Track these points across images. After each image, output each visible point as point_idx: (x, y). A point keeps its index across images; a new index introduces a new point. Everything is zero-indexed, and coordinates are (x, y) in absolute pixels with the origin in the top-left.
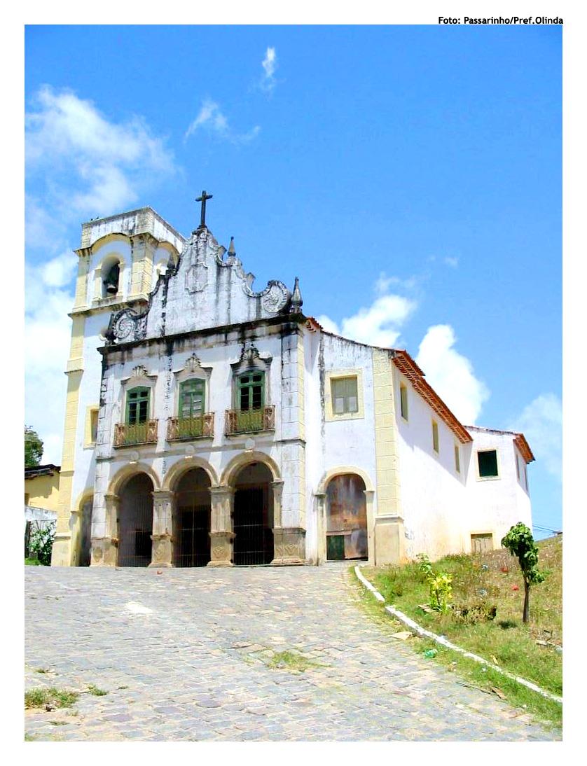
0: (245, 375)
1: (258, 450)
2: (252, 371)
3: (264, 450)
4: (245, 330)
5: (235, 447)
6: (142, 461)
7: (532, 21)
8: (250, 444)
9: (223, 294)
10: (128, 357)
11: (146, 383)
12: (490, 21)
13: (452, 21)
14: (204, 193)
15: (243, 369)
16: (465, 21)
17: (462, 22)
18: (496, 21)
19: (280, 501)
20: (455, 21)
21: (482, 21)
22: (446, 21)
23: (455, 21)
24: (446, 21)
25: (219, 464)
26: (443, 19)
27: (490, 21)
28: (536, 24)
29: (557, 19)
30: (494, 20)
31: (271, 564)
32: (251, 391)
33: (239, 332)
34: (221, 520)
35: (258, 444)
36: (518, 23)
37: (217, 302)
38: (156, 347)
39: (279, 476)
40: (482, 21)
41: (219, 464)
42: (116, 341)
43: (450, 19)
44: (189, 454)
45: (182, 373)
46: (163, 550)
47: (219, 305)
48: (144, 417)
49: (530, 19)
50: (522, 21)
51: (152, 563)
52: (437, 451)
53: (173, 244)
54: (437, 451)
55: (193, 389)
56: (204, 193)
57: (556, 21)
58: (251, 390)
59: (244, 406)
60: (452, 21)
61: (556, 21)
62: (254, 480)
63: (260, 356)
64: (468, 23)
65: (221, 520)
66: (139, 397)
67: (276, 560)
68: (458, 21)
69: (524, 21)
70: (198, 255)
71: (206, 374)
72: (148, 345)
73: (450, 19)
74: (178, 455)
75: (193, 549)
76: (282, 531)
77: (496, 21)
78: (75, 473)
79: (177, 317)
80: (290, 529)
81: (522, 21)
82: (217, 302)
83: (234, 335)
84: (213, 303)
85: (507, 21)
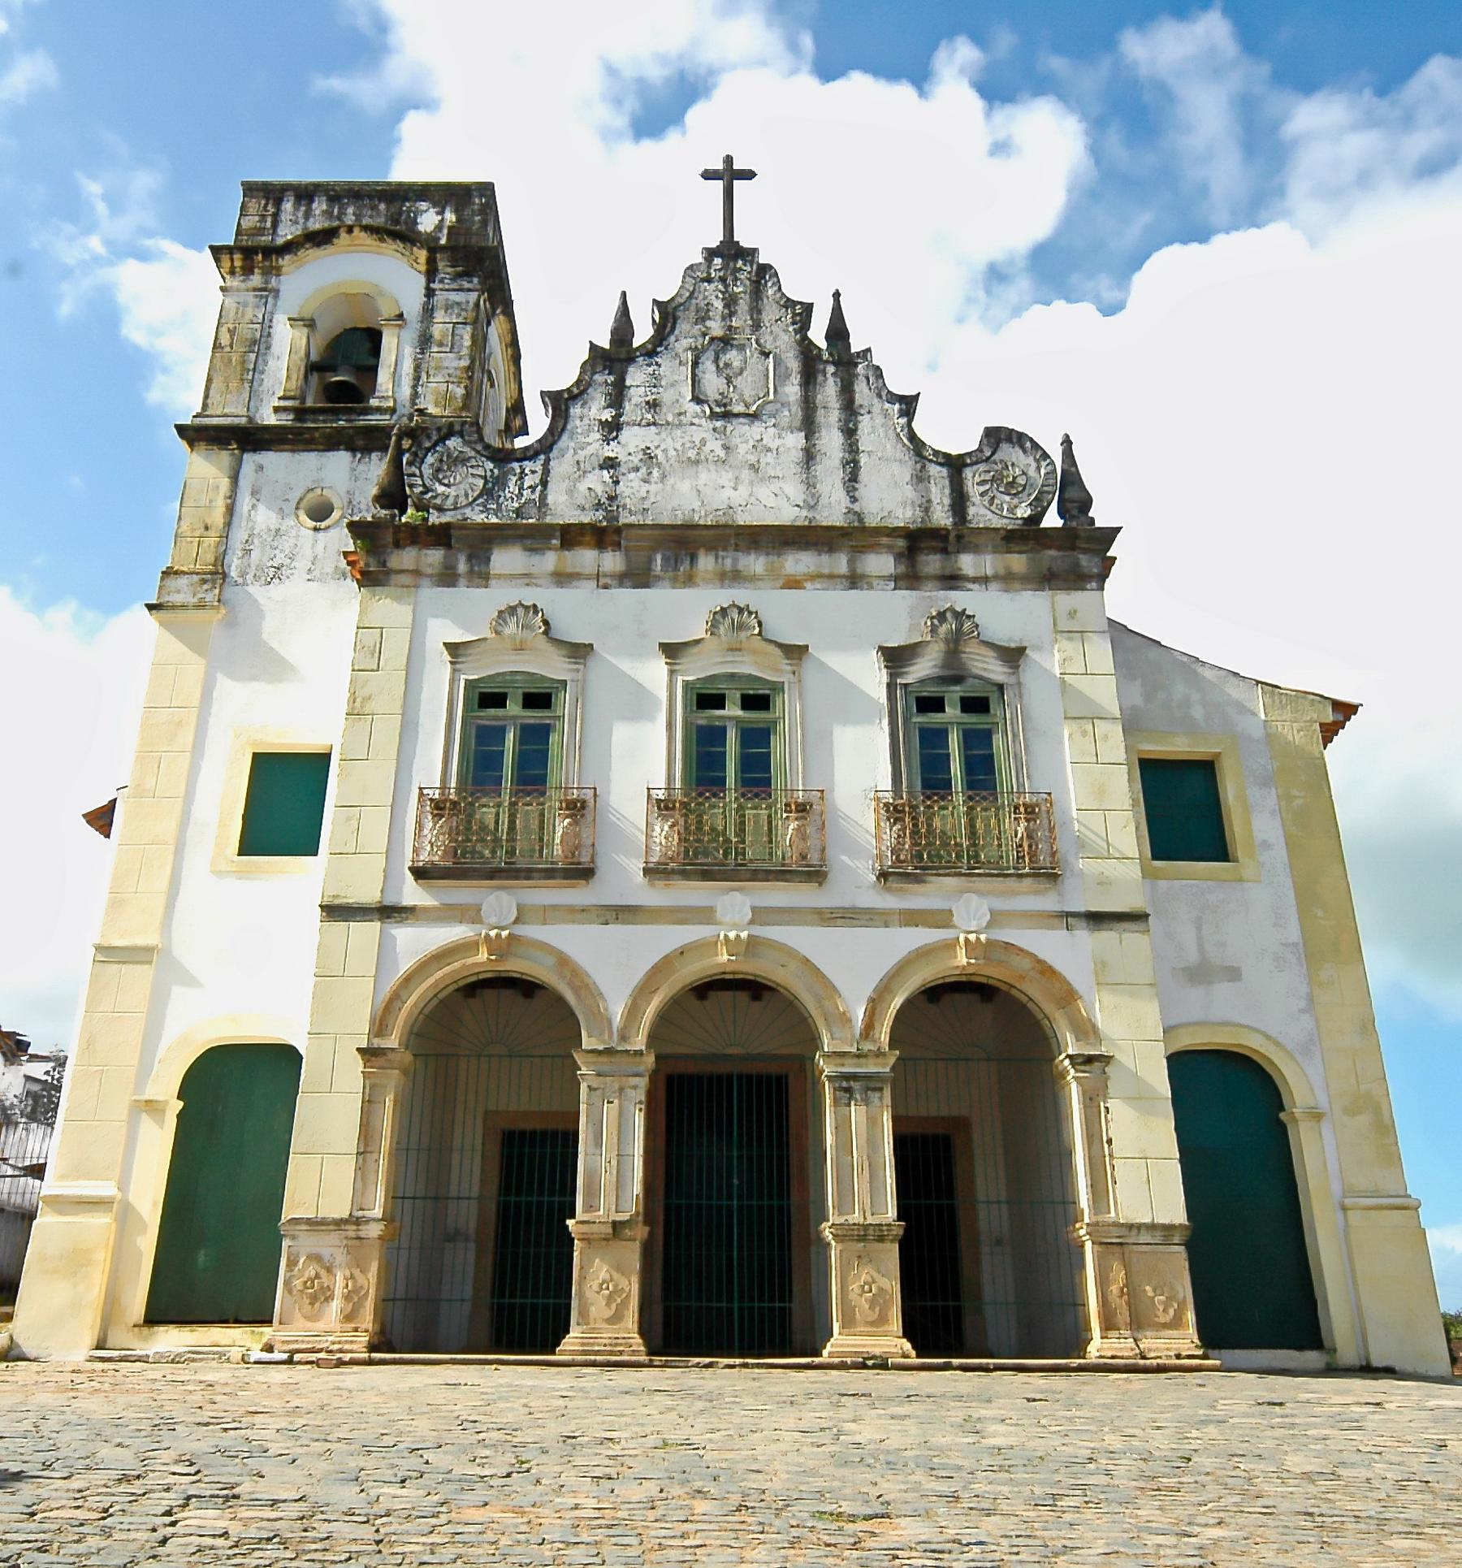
0: (931, 691)
2: (958, 680)
5: (911, 918)
6: (532, 931)
9: (831, 440)
10: (471, 572)
11: (550, 666)
14: (729, 160)
15: (921, 669)
25: (853, 971)
31: (825, 1358)
33: (898, 557)
34: (856, 1170)
35: (760, 915)
37: (809, 456)
38: (586, 558)
41: (853, 971)
42: (410, 515)
44: (727, 924)
45: (696, 650)
46: (606, 1288)
47: (819, 469)
48: (533, 773)
51: (571, 1334)
56: (729, 160)
58: (732, 736)
59: (935, 782)
62: (735, 1038)
65: (856, 1170)
66: (733, 710)
67: (839, 1343)
70: (731, 314)
71: (784, 664)
72: (556, 542)
75: (730, 1290)
76: (1123, 1232)
79: (663, 477)
80: (1152, 1227)
82: (809, 456)
84: (797, 455)
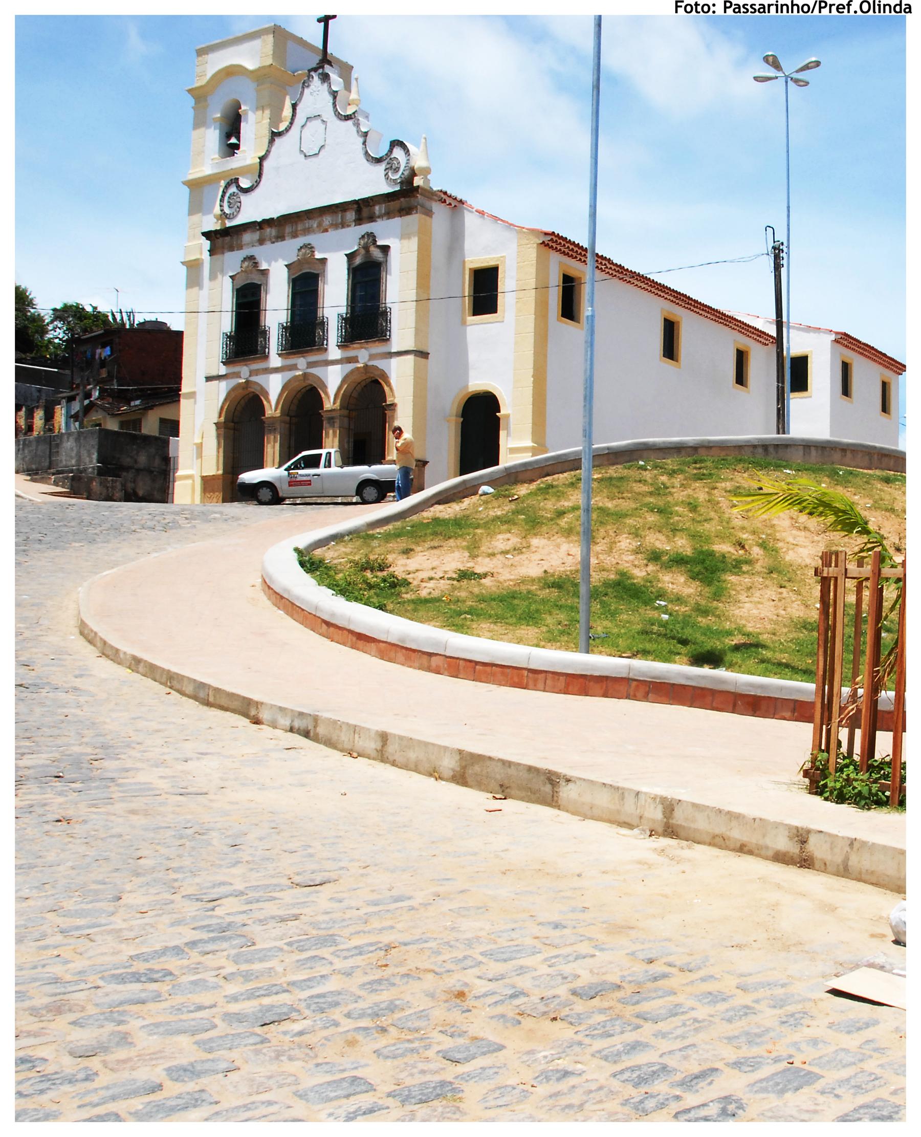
1: (370, 363)
3: (380, 364)
4: (362, 210)
6: (253, 379)
7: (852, 9)
8: (363, 354)
12: (773, 9)
13: (699, 9)
16: (726, 8)
17: (719, 9)
18: (785, 8)
19: (389, 385)
20: (706, 9)
21: (757, 7)
22: (689, 9)
23: (706, 9)
24: (689, 9)
26: (683, 5)
27: (773, 9)
28: (859, 13)
29: (900, 5)
30: (780, 8)
32: (367, 275)
36: (825, 11)
39: (393, 395)
40: (757, 7)
43: (697, 4)
49: (849, 5)
50: (834, 8)
52: (828, 992)
53: (430, 1104)
54: (828, 992)
55: (305, 286)
57: (898, 9)
60: (699, 9)
61: (898, 9)
63: (379, 243)
64: (730, 11)
68: (712, 9)
69: (838, 9)
73: (697, 4)
74: (290, 370)
77: (785, 8)
78: (191, 126)
81: (834, 8)
83: (351, 215)
85: (806, 9)
